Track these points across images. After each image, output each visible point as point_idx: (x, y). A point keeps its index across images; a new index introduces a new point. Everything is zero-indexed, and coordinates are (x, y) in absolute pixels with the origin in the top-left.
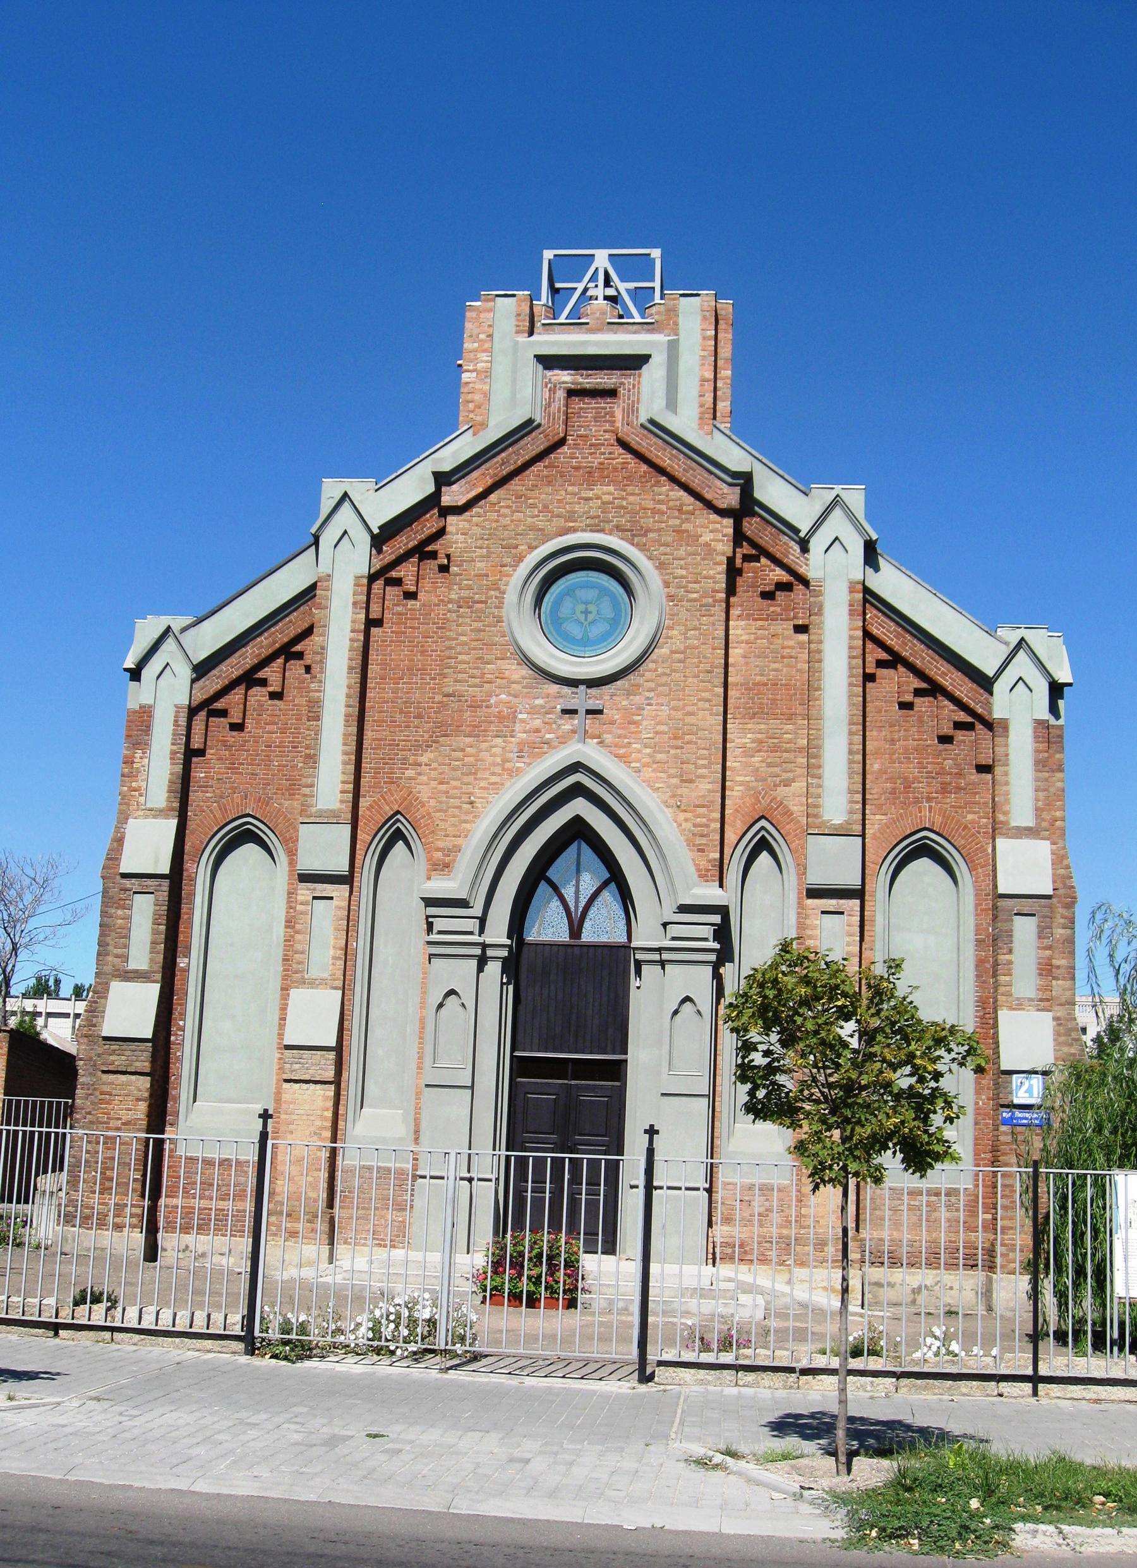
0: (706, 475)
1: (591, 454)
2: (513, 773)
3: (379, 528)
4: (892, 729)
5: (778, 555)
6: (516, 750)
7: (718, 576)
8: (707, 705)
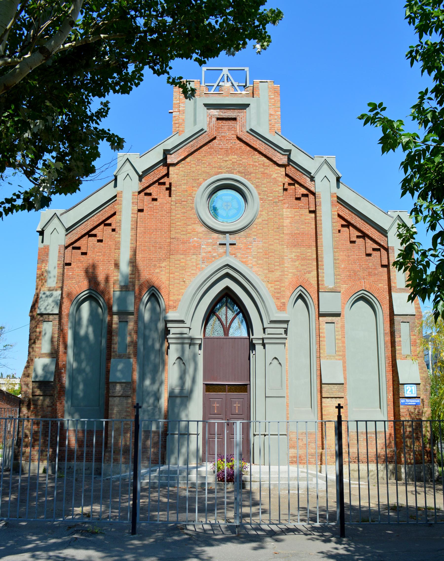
0: (273, 151)
1: (227, 143)
2: (202, 269)
3: (142, 172)
4: (348, 251)
5: (302, 183)
6: (202, 260)
7: (280, 191)
8: (278, 241)
